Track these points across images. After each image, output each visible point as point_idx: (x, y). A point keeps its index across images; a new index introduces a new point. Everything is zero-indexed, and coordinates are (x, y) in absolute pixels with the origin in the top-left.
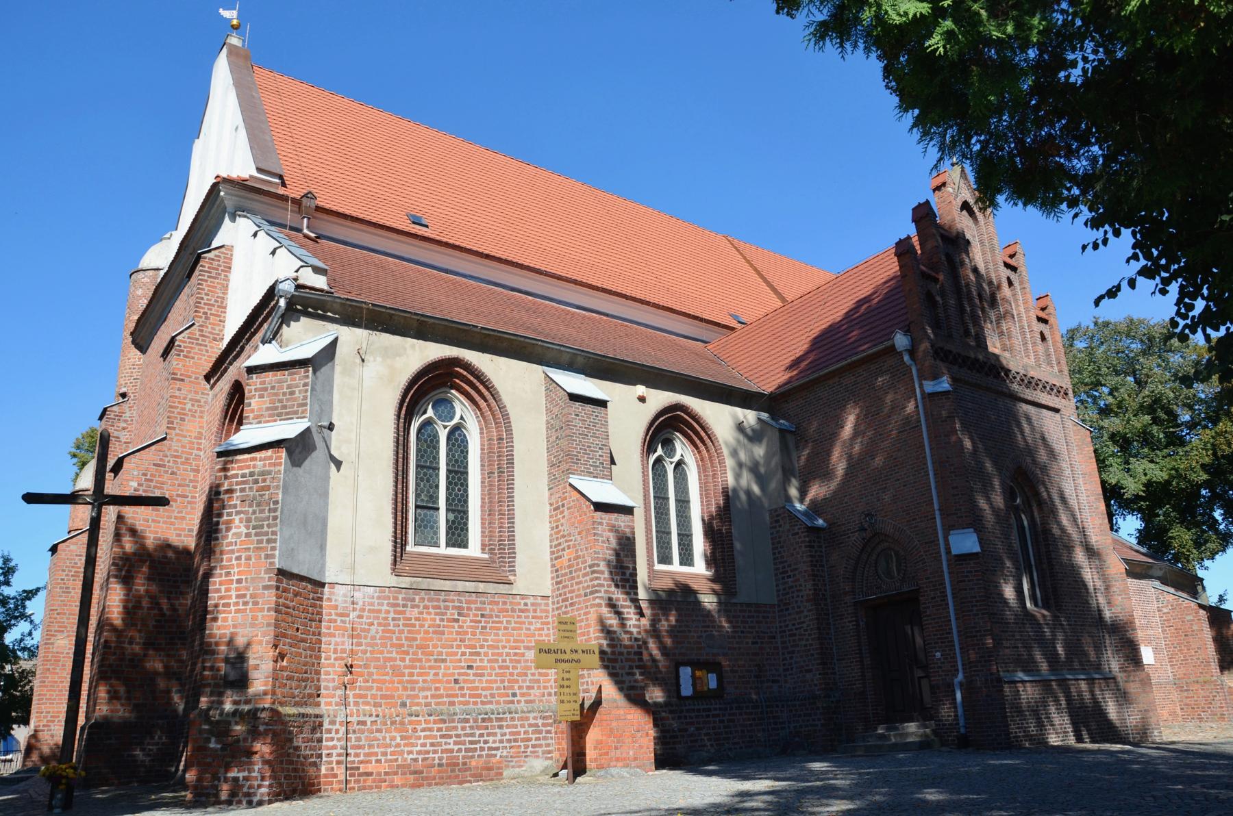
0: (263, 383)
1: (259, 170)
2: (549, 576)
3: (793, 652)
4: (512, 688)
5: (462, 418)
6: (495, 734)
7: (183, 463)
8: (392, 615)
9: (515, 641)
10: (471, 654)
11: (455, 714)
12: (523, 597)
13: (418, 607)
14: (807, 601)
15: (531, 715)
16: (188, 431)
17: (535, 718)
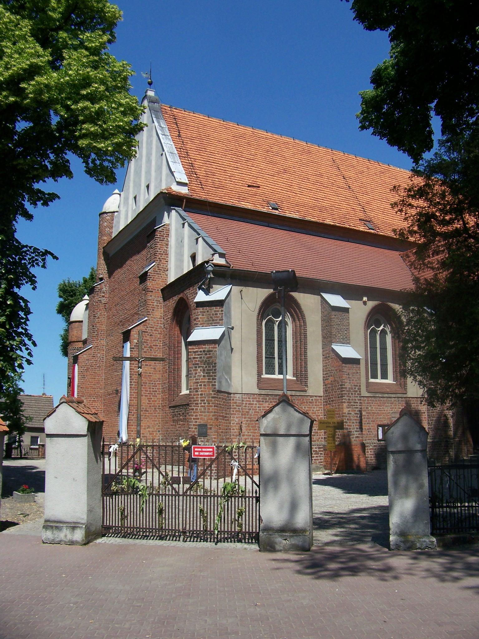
2: (322, 387)
7: (155, 331)
8: (258, 405)
13: (268, 402)
16: (156, 315)
17: (316, 448)
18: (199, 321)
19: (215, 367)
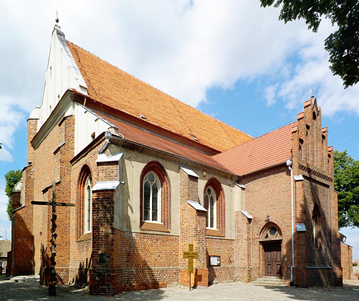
0: (103, 168)
3: (239, 254)
4: (169, 262)
5: (156, 181)
6: (165, 275)
8: (140, 241)
9: (170, 249)
10: (160, 252)
11: (156, 269)
14: (245, 240)
15: (174, 270)
17: (175, 271)
18: (100, 177)
19: (113, 210)
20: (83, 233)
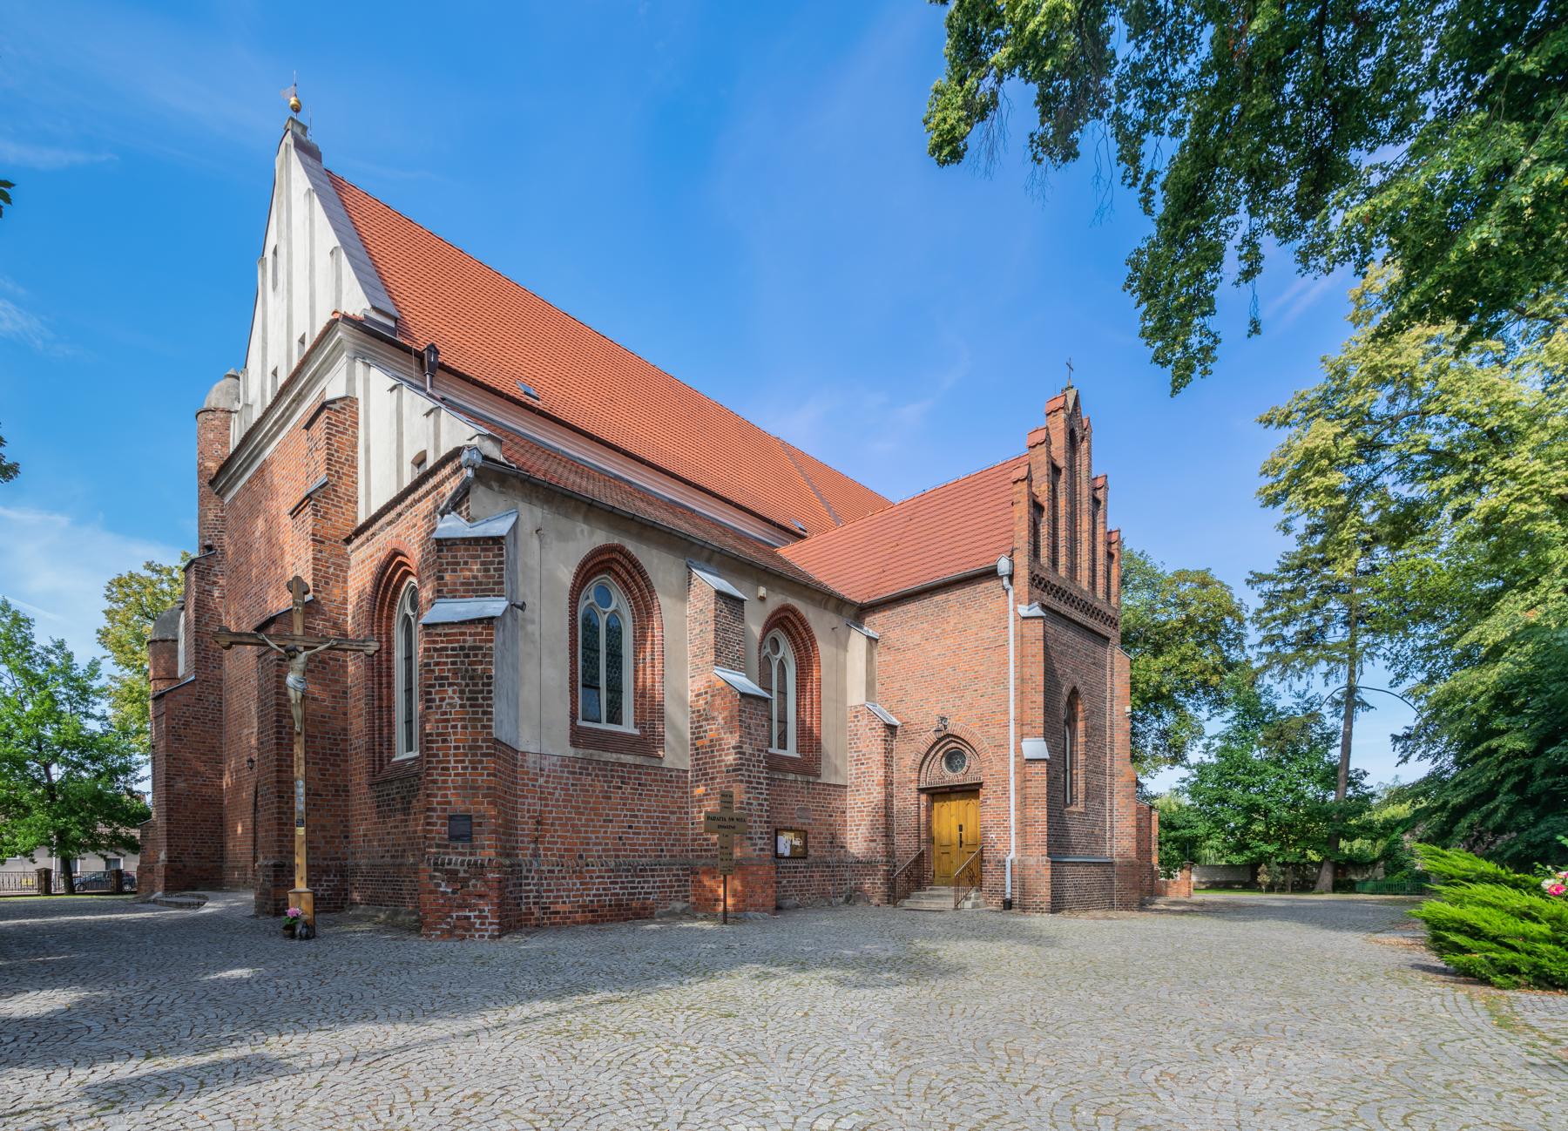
1: (374, 308)
12: (670, 770)
19: (489, 685)
20: (390, 757)
